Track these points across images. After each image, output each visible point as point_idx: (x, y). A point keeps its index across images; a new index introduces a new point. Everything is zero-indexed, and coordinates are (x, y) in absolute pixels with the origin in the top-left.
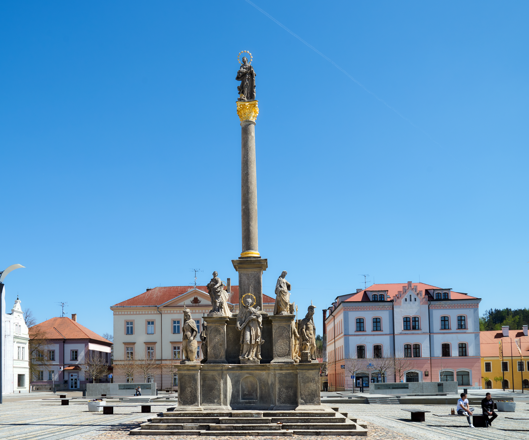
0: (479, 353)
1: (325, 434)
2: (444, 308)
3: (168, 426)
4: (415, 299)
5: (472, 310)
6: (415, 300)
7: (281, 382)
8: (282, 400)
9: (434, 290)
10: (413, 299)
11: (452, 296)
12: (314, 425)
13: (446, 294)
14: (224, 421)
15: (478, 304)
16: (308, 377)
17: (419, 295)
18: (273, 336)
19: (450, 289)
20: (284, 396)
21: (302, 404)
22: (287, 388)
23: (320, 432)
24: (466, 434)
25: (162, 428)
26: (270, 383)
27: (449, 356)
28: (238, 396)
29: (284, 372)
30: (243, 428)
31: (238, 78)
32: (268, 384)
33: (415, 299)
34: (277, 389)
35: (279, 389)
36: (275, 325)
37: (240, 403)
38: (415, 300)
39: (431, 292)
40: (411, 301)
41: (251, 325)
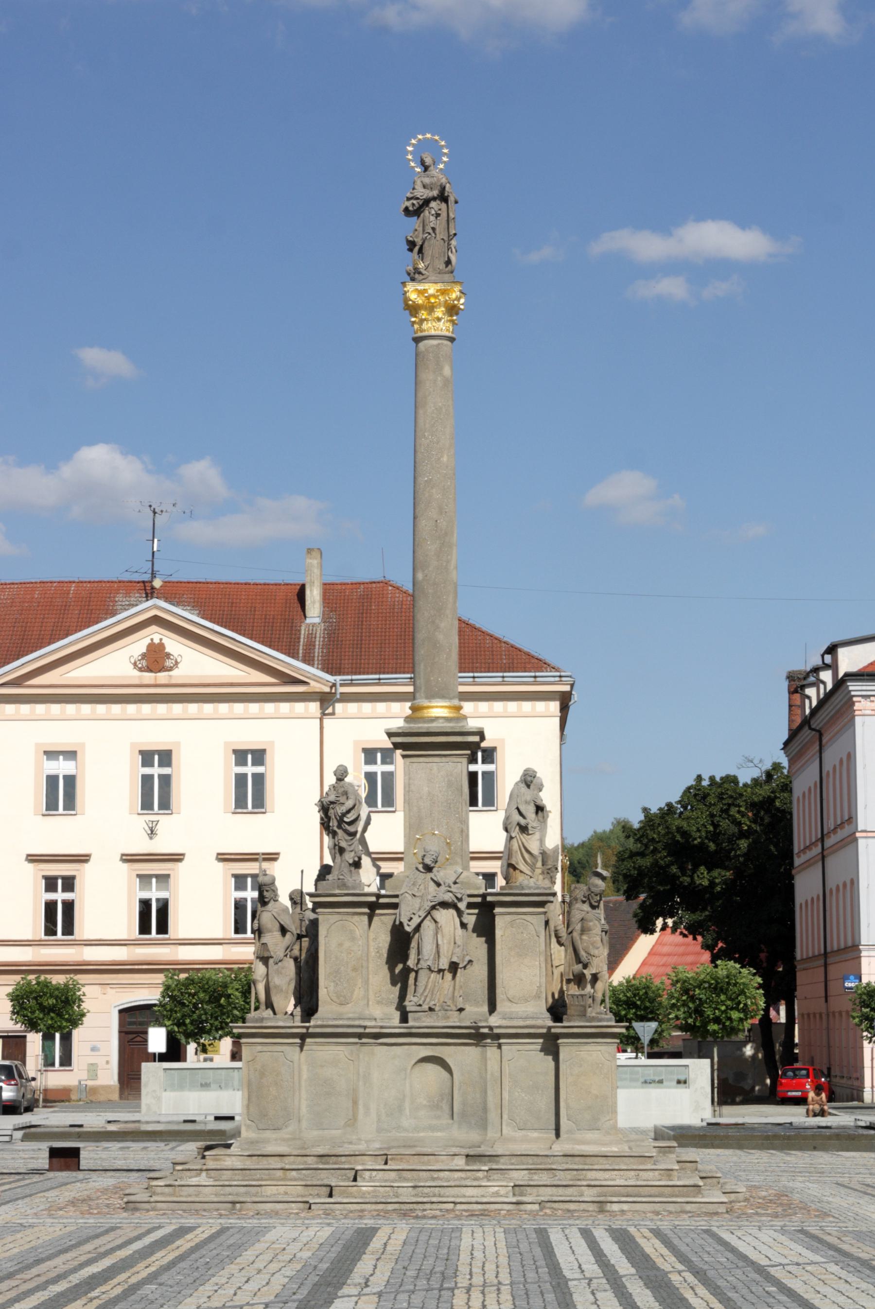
28: (400, 1109)
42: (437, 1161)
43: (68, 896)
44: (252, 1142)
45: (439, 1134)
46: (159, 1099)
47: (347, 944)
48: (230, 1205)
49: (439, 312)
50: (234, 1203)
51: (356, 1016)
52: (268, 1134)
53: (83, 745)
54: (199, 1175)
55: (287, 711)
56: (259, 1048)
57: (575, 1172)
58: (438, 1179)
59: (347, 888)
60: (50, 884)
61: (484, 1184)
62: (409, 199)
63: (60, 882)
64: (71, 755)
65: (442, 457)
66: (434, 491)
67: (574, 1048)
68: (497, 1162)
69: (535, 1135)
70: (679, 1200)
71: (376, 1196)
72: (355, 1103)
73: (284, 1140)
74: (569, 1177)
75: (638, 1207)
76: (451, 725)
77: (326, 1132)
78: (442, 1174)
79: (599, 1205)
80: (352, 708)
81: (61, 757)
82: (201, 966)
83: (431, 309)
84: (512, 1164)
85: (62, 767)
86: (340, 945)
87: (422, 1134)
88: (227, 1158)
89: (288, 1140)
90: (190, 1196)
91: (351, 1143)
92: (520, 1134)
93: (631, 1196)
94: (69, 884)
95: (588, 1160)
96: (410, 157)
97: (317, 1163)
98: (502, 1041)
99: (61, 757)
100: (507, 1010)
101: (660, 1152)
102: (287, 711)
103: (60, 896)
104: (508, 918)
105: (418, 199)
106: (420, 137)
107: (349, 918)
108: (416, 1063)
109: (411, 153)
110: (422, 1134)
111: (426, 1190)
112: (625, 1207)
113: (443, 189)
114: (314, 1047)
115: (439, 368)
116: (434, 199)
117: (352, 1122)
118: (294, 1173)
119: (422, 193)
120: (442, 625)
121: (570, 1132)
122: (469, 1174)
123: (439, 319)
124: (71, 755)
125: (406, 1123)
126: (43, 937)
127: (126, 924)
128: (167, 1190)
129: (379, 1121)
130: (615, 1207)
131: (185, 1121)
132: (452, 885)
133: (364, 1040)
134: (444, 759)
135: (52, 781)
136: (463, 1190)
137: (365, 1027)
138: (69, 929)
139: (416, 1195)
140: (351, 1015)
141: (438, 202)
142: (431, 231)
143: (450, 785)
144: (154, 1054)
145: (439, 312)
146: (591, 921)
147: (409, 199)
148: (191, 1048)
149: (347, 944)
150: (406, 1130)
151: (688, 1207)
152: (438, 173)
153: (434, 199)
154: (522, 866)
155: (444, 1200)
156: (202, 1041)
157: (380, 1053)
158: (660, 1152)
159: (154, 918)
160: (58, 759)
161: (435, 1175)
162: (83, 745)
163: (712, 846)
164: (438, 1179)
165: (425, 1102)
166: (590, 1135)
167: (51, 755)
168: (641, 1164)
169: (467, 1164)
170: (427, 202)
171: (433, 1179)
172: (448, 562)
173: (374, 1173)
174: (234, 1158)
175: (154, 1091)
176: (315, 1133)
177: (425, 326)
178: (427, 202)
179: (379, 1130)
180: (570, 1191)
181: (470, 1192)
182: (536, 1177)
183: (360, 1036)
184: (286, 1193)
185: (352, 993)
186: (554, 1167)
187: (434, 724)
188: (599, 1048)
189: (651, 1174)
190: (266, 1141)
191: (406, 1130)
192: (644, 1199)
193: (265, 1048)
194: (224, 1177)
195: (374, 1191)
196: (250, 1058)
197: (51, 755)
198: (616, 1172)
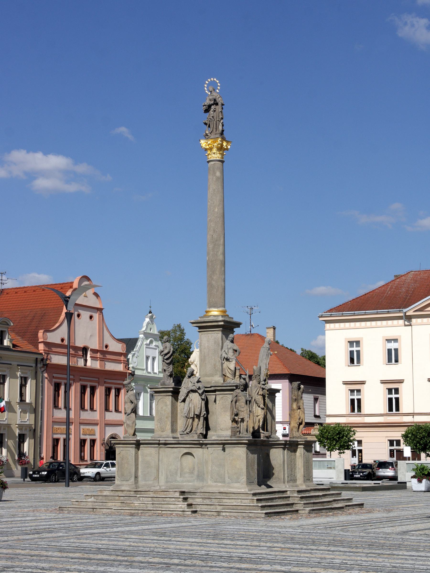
28: (176, 473)
42: (169, 494)
43: (397, 396)
44: (118, 486)
45: (191, 484)
46: (405, 475)
47: (164, 408)
48: (92, 509)
49: (215, 150)
50: (93, 509)
51: (167, 436)
52: (124, 483)
53: (400, 336)
54: (91, 498)
55: (426, 321)
56: (121, 449)
57: (219, 500)
58: (165, 501)
59: (165, 385)
60: (390, 391)
61: (176, 503)
62: (204, 106)
63: (393, 390)
64: (396, 340)
65: (215, 209)
66: (212, 223)
67: (231, 449)
68: (196, 495)
69: (220, 484)
70: (247, 511)
71: (140, 507)
72: (158, 471)
73: (129, 485)
74: (217, 501)
75: (232, 514)
76: (215, 318)
77: (147, 482)
78: (167, 499)
79: (217, 513)
80: (419, 320)
81: (393, 342)
82: (410, 424)
83: (211, 149)
84: (201, 496)
85: (392, 346)
86: (162, 408)
87: (184, 484)
88: (105, 492)
89: (131, 485)
90: (84, 505)
91: (154, 487)
92: (215, 484)
93: (234, 510)
94: (397, 391)
95: (228, 494)
96: (219, 88)
97: (134, 494)
98: (208, 446)
99: (393, 342)
100: (220, 434)
101: (291, 493)
102: (426, 321)
103: (394, 396)
104: (221, 396)
105: (205, 105)
106: (215, 79)
107: (165, 397)
108: (183, 455)
109: (218, 86)
110: (184, 484)
111: (157, 505)
112: (227, 514)
113: (215, 100)
114: (143, 449)
115: (214, 173)
116: (213, 104)
117: (157, 478)
118: (122, 498)
119: (208, 102)
120: (215, 278)
122: (176, 499)
123: (214, 153)
124: (396, 340)
125: (178, 479)
126: (388, 413)
127: (383, 408)
128: (77, 503)
129: (167, 478)
130: (224, 514)
131: (342, 483)
132: (196, 383)
133: (161, 446)
134: (213, 332)
135: (389, 351)
136: (170, 506)
137: (159, 441)
138: (397, 409)
139: (153, 507)
140: (165, 436)
141: (215, 106)
142: (212, 118)
143: (215, 342)
144: (406, 457)
145: (215, 150)
146: (240, 396)
147: (204, 106)
148: (423, 455)
149: (164, 408)
150: (178, 482)
151: (251, 515)
152: (215, 95)
153: (213, 104)
154: (228, 375)
155: (158, 509)
156: (427, 453)
157: (166, 452)
158: (291, 493)
159: (393, 405)
160: (391, 342)
161: (165, 499)
162: (400, 336)
163: (186, 364)
164: (165, 501)
165: (188, 471)
166: (236, 485)
167: (389, 341)
168: (247, 497)
169: (180, 495)
170: (210, 106)
171: (164, 501)
172: (217, 252)
173: (144, 498)
174: (107, 492)
175: (403, 472)
176: (144, 482)
177: (209, 156)
178: (210, 106)
179: (167, 482)
180: (212, 507)
181: (172, 506)
182: (205, 501)
183: (159, 444)
184: (115, 506)
185: (166, 427)
186: (211, 497)
187: (210, 318)
188: (239, 449)
189: (246, 501)
190: (122, 485)
191: (178, 482)
192: (234, 511)
193: (124, 449)
194: (99, 499)
195: (139, 505)
196: (119, 453)
197: (389, 341)
198: (233, 500)
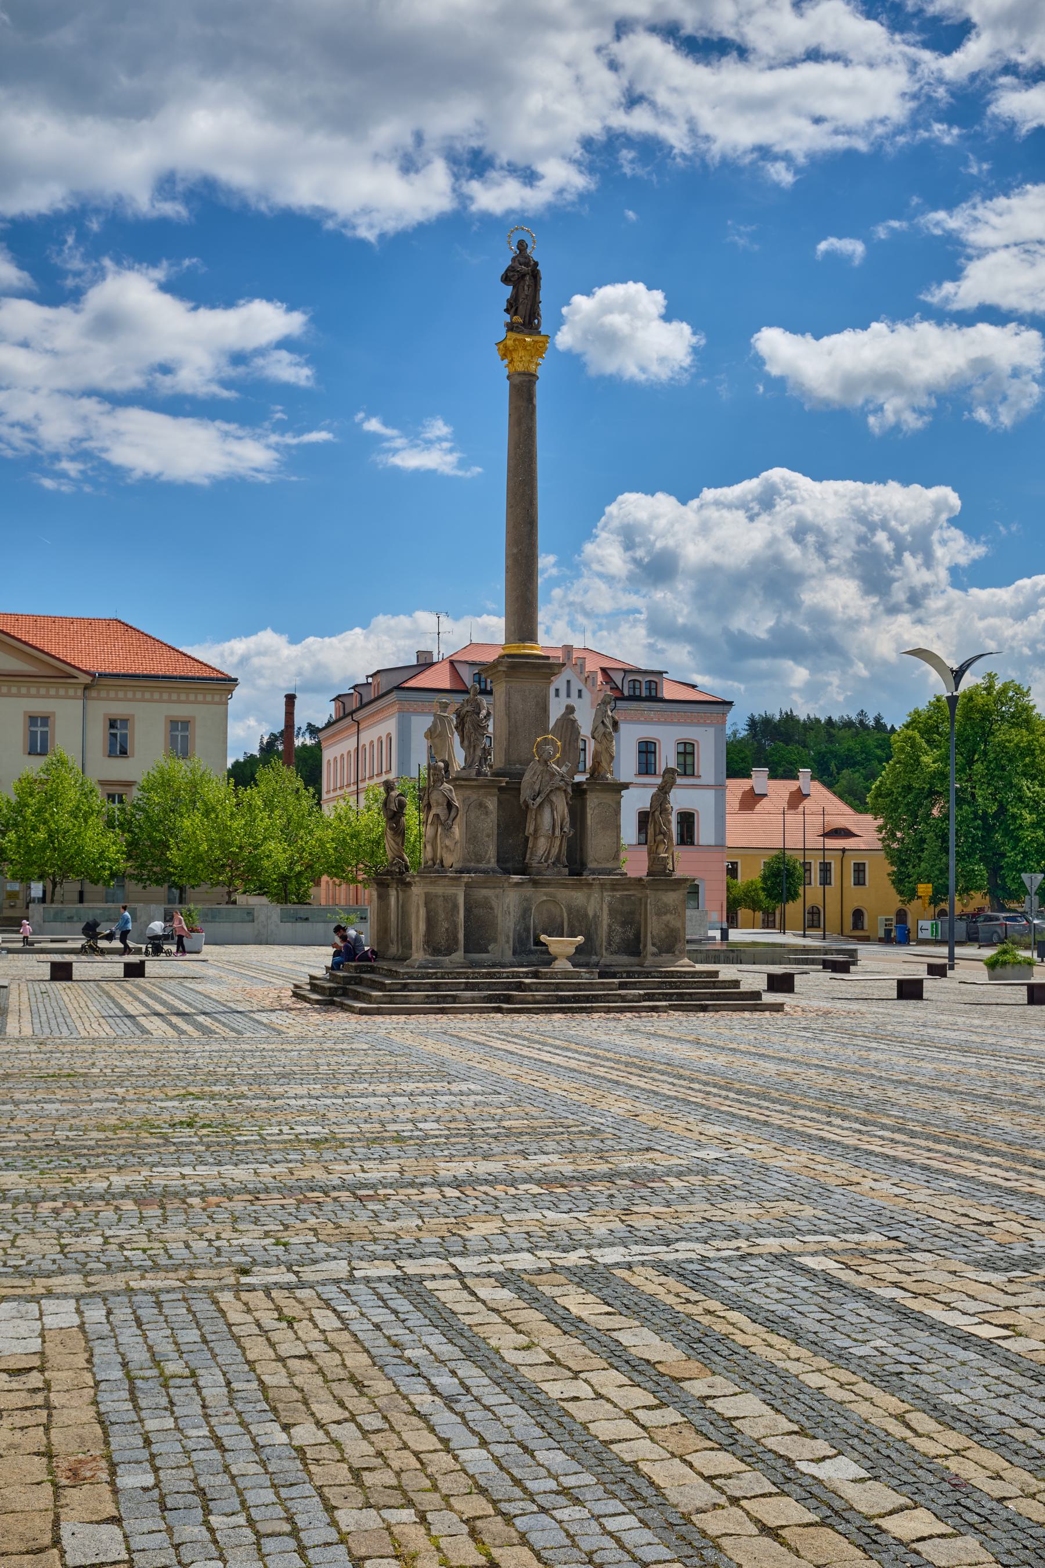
0: (723, 838)
1: (717, 1009)
2: (648, 721)
3: (428, 996)
4: (580, 691)
5: (711, 731)
6: (580, 696)
7: (612, 912)
8: (614, 947)
9: (625, 671)
10: (574, 693)
11: (669, 692)
12: (690, 994)
13: (653, 686)
14: (534, 987)
15: (724, 714)
16: (666, 905)
17: (590, 682)
18: (589, 822)
19: (661, 673)
20: (617, 939)
21: (653, 954)
22: (624, 924)
23: (707, 1005)
24: (562, 1048)
25: (414, 1000)
26: (591, 914)
27: (692, 843)
28: (528, 938)
29: (618, 894)
30: (576, 999)
31: (506, 279)
32: (586, 915)
33: (580, 691)
34: (605, 927)
35: (610, 926)
36: (593, 801)
37: (531, 952)
38: (580, 696)
39: (618, 678)
40: (568, 696)
41: (554, 799)
121: (653, 954)
